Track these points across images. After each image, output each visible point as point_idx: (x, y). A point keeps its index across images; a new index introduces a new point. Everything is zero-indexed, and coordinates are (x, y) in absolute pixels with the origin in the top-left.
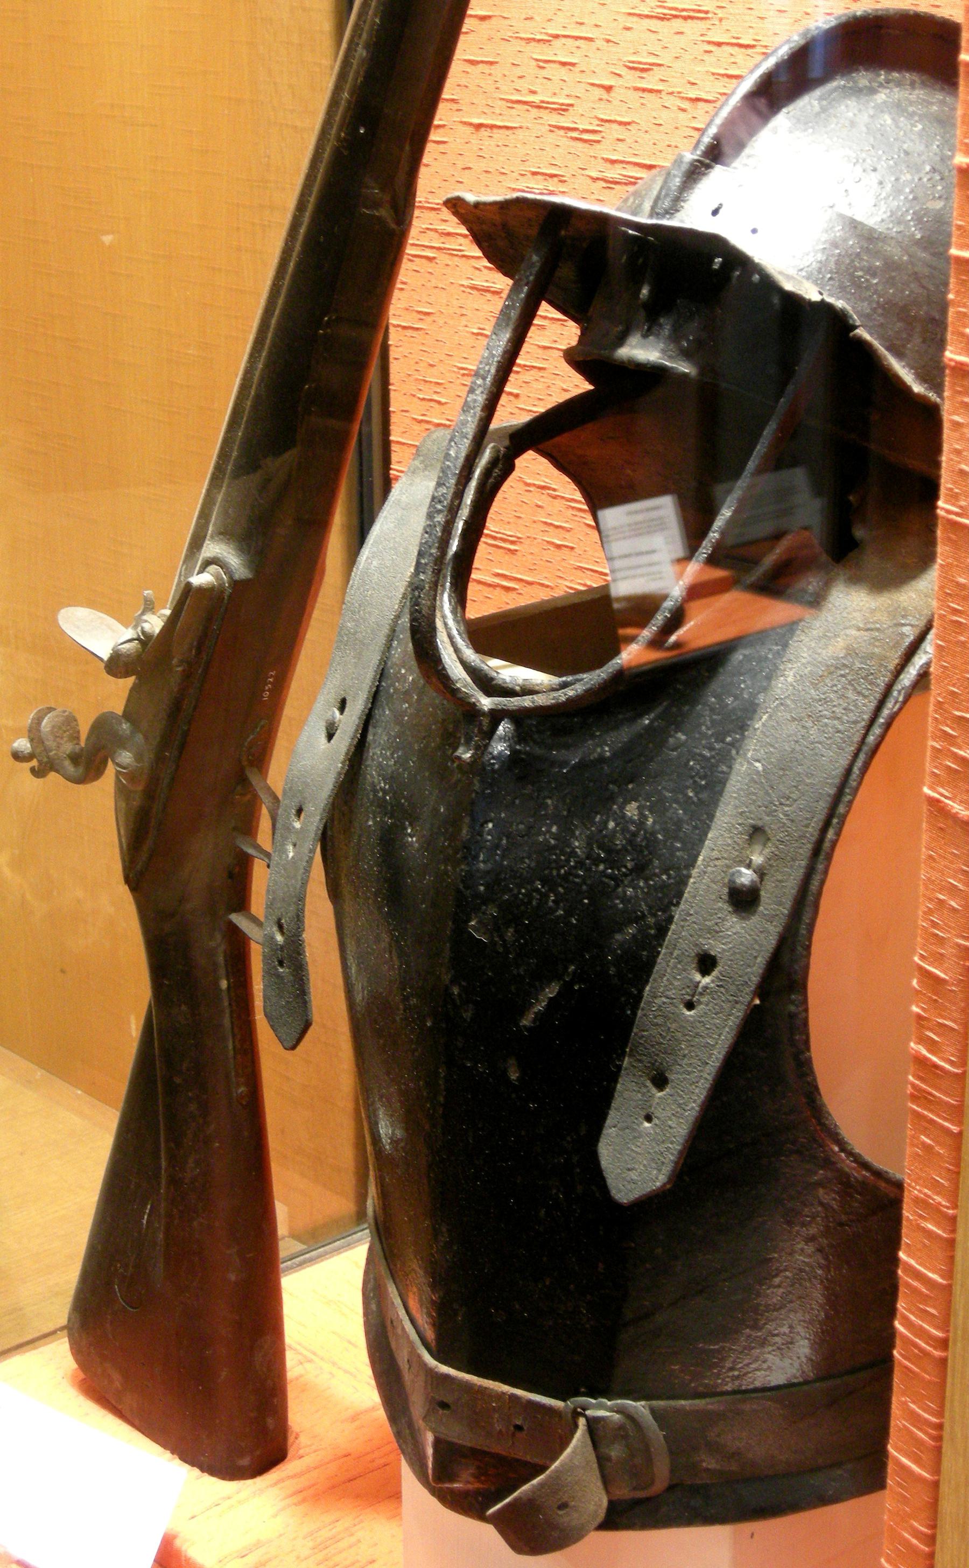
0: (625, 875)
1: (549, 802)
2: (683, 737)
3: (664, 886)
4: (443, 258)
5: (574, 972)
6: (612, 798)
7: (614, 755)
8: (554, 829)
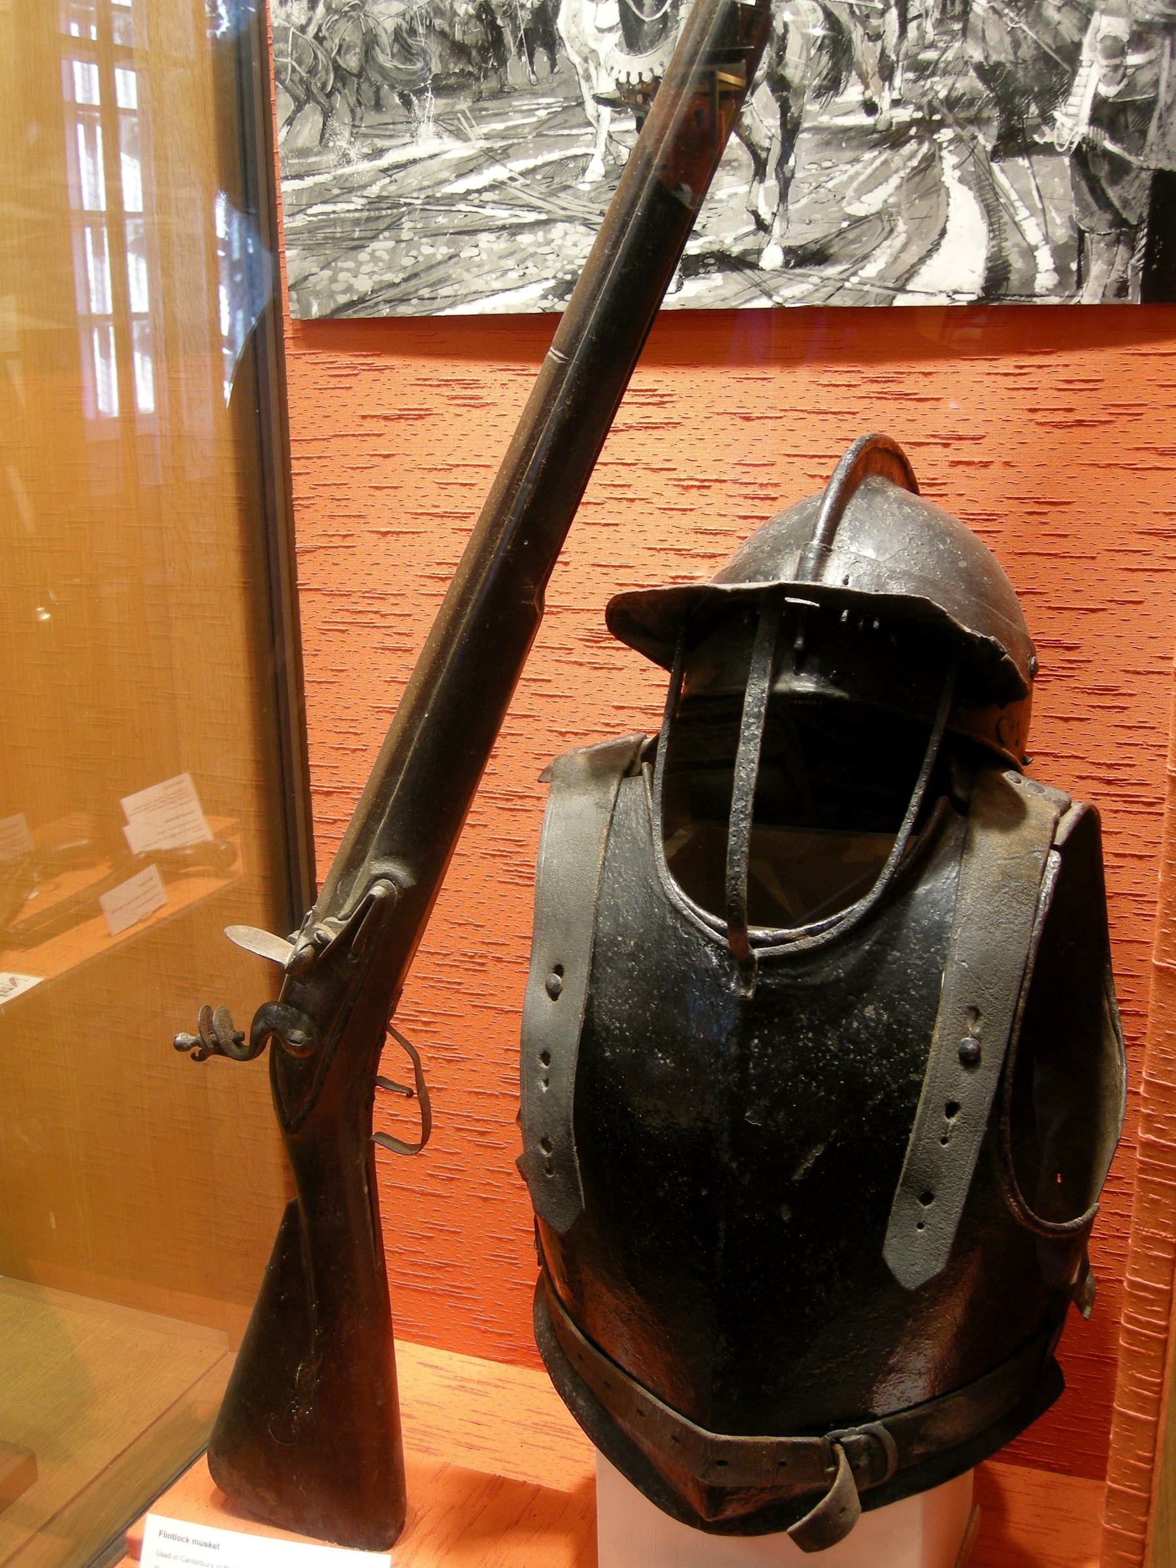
0: (871, 1058)
1: (802, 1016)
2: (898, 954)
3: (902, 1060)
4: (355, 630)
5: (836, 1134)
6: (852, 1006)
7: (847, 975)
8: (810, 1035)
